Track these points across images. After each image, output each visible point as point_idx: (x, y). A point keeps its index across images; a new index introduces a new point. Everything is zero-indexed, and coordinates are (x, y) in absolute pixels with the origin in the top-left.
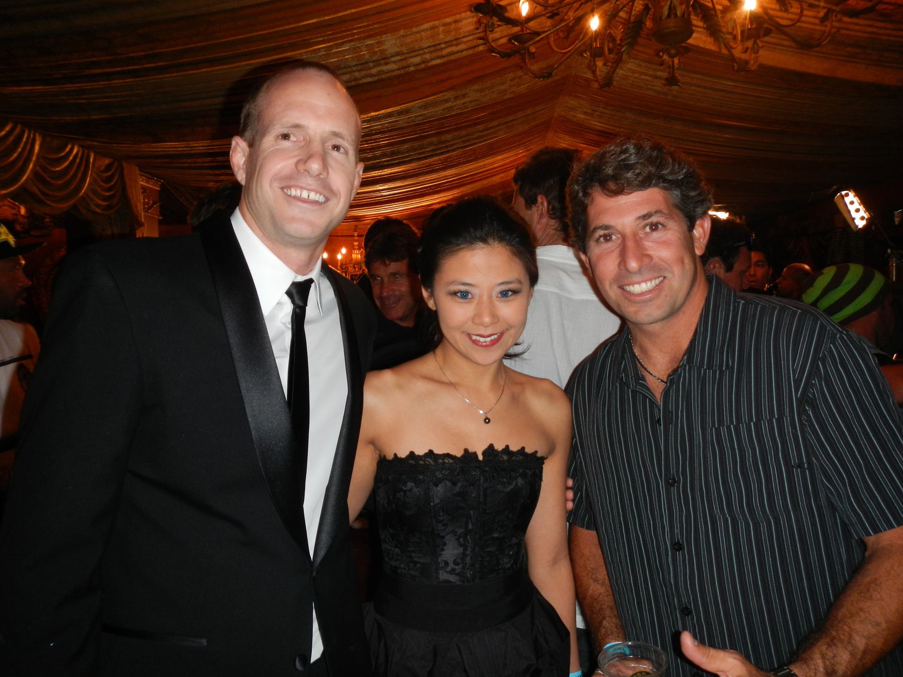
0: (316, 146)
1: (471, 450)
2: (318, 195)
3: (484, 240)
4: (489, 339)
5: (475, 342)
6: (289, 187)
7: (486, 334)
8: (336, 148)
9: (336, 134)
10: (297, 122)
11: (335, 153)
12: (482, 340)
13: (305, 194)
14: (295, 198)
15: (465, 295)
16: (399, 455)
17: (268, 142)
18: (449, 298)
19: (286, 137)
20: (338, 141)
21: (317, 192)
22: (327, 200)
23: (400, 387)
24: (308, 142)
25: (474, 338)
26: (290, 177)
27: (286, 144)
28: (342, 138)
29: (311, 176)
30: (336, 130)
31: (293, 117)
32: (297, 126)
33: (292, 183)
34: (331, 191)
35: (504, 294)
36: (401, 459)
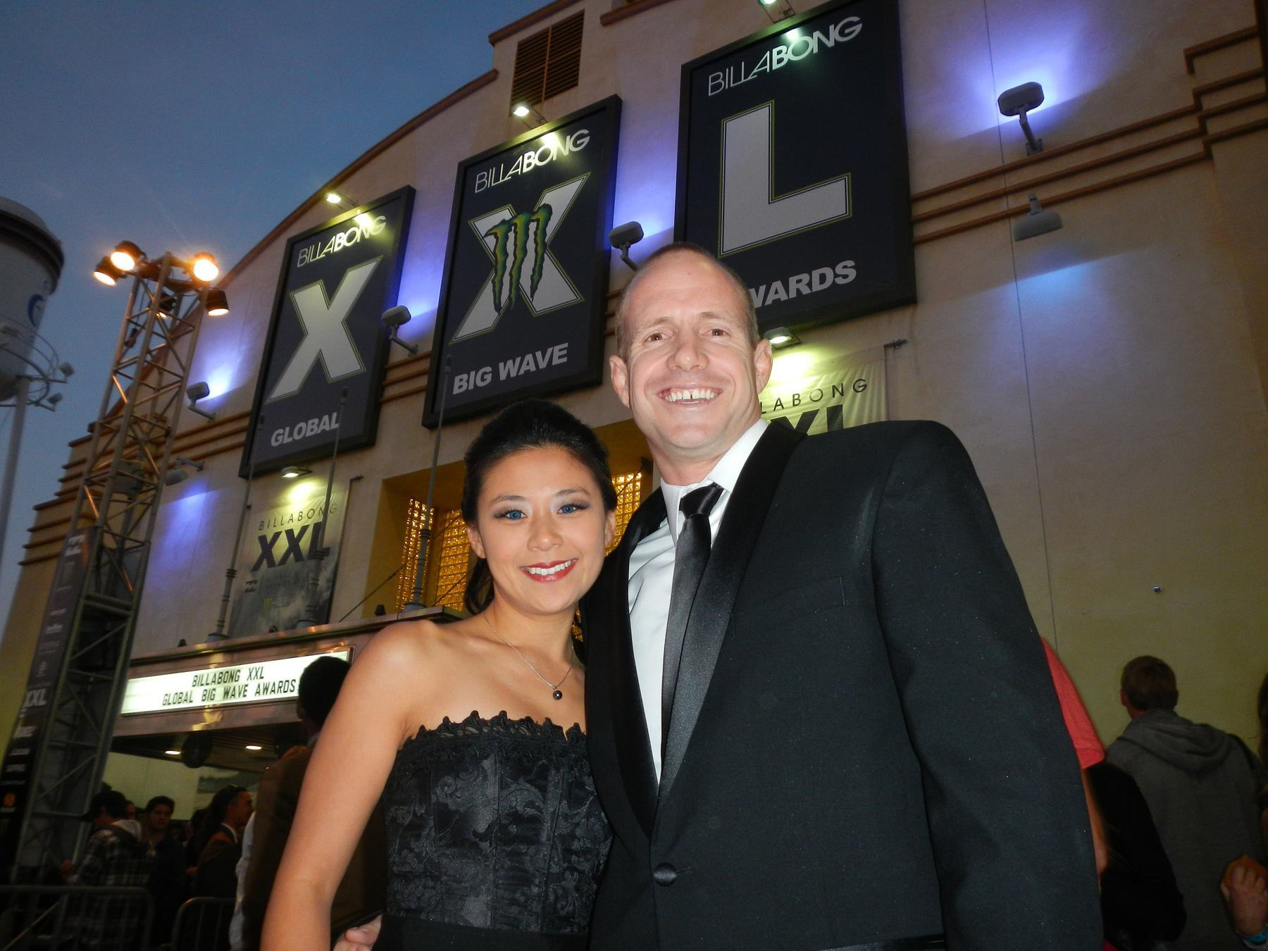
0: (687, 334)
1: (555, 722)
2: (703, 392)
3: (536, 443)
4: (552, 570)
5: (537, 578)
6: (668, 391)
7: (547, 561)
8: (718, 332)
9: (708, 315)
10: (659, 316)
11: (717, 339)
12: (543, 572)
13: (687, 395)
14: (677, 402)
15: (515, 514)
16: (427, 728)
17: (637, 349)
18: (496, 521)
19: (656, 337)
20: (717, 324)
21: (700, 387)
22: (719, 392)
23: (445, 642)
24: (677, 333)
25: (533, 571)
26: (664, 379)
27: (658, 343)
28: (717, 317)
29: (685, 371)
30: (706, 310)
31: (655, 311)
32: (661, 321)
33: (667, 385)
34: (721, 380)
35: (567, 509)
36: (431, 732)
